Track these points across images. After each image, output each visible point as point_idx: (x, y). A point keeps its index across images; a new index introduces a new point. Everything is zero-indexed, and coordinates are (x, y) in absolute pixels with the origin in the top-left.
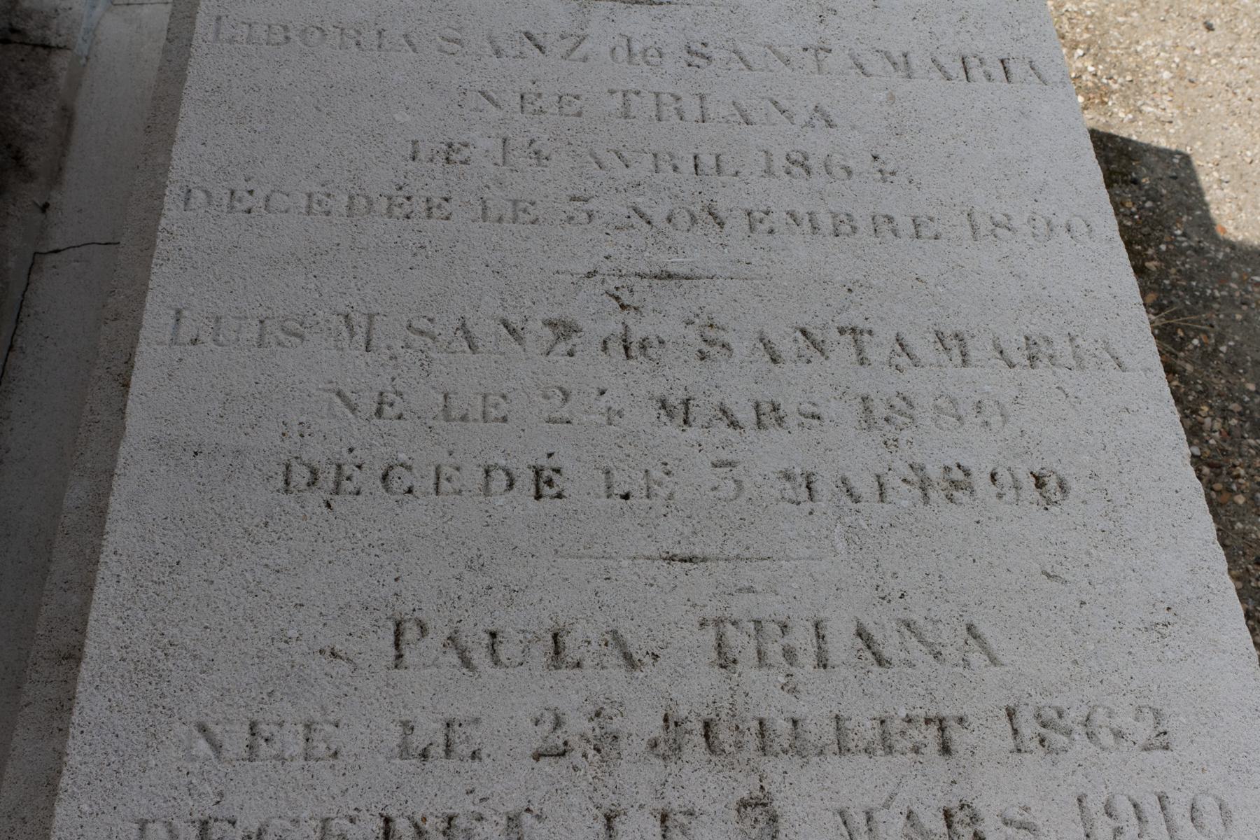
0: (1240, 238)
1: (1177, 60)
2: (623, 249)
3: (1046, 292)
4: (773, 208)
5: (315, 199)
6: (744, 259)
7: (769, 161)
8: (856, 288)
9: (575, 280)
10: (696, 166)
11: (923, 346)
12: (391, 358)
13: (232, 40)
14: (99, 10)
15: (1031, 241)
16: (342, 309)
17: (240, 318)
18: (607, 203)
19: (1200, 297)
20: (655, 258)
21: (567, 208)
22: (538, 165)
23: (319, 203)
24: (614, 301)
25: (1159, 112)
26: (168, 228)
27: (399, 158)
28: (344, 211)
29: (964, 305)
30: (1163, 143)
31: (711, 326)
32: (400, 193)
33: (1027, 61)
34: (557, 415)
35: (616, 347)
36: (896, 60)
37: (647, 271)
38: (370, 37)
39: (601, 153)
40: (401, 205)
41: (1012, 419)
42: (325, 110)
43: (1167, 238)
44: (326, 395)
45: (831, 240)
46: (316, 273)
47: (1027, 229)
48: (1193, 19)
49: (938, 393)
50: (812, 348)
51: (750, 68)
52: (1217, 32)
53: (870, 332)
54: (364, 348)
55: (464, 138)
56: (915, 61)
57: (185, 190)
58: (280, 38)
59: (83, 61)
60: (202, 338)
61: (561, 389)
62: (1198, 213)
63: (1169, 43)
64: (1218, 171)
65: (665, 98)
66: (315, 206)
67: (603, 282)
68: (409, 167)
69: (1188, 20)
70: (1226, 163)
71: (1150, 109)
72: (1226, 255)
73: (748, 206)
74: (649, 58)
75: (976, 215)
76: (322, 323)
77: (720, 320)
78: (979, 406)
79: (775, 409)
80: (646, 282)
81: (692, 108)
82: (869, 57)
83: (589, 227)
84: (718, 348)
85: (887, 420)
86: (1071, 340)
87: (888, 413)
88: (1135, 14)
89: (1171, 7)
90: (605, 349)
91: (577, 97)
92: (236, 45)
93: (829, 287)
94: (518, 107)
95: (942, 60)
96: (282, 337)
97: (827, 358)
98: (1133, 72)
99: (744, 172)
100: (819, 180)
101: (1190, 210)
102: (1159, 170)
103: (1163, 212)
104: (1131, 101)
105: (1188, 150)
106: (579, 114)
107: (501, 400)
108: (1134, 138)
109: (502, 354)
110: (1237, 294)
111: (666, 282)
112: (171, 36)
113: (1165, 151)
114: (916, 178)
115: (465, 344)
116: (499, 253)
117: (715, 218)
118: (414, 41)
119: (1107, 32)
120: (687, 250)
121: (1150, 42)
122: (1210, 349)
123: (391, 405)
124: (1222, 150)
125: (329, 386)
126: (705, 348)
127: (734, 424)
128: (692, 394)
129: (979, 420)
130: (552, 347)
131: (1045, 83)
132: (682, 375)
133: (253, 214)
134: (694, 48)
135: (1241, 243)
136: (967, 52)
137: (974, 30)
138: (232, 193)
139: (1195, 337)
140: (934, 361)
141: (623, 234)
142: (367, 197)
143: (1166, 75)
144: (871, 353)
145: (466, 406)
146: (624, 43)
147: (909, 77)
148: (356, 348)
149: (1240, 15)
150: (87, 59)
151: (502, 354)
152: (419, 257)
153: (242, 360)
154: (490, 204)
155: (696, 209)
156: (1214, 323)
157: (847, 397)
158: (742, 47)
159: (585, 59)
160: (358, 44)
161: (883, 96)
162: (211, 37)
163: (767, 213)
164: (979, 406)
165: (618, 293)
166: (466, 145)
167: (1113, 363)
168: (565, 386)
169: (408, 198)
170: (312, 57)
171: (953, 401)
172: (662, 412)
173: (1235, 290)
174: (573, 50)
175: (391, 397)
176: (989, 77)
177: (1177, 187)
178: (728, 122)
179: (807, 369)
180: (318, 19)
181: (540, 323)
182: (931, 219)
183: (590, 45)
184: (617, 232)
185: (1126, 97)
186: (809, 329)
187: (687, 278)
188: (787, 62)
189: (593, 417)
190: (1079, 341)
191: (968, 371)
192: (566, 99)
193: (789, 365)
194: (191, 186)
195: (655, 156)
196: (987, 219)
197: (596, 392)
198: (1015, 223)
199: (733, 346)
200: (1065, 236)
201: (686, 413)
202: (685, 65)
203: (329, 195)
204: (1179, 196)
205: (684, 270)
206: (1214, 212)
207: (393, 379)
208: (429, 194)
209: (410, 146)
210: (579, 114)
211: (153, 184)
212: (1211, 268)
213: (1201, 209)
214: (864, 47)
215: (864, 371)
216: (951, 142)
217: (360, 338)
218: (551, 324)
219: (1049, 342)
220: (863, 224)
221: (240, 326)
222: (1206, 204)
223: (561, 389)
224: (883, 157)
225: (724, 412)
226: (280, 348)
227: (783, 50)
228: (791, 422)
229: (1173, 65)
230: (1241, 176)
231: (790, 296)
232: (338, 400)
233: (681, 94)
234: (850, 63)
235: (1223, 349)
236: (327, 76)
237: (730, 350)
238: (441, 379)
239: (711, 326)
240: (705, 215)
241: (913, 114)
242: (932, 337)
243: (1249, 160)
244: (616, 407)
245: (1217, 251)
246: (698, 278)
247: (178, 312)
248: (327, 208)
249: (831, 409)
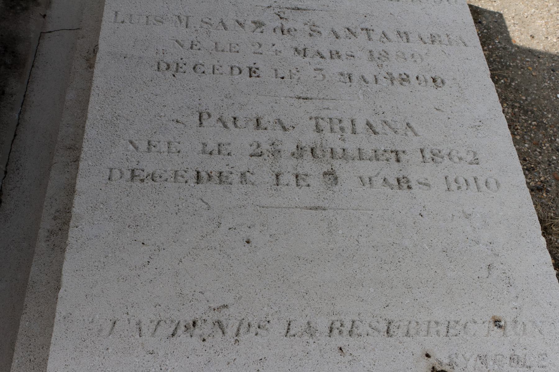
0: (521, 45)
8: (368, 16)
16: (177, 14)
30: (492, 9)
43: (492, 43)
53: (373, 30)
61: (258, 43)
70: (517, 17)
72: (515, 50)
78: (413, 55)
79: (337, 53)
80: (289, 10)
96: (155, 22)
108: (480, 7)
113: (492, 12)
126: (312, 32)
132: (303, 41)
135: (522, 46)
164: (413, 55)
168: (260, 42)
175: (196, 43)
177: (497, 25)
179: (349, 41)
193: (342, 40)
197: (271, 45)
199: (322, 32)
205: (304, 7)
206: (511, 35)
212: (509, 55)
215: (370, 42)
217: (184, 23)
218: (255, 23)
219: (439, 36)
228: (344, 57)
230: (523, 22)
235: (513, 84)
242: (396, 33)
245: (512, 49)
247: (116, 12)
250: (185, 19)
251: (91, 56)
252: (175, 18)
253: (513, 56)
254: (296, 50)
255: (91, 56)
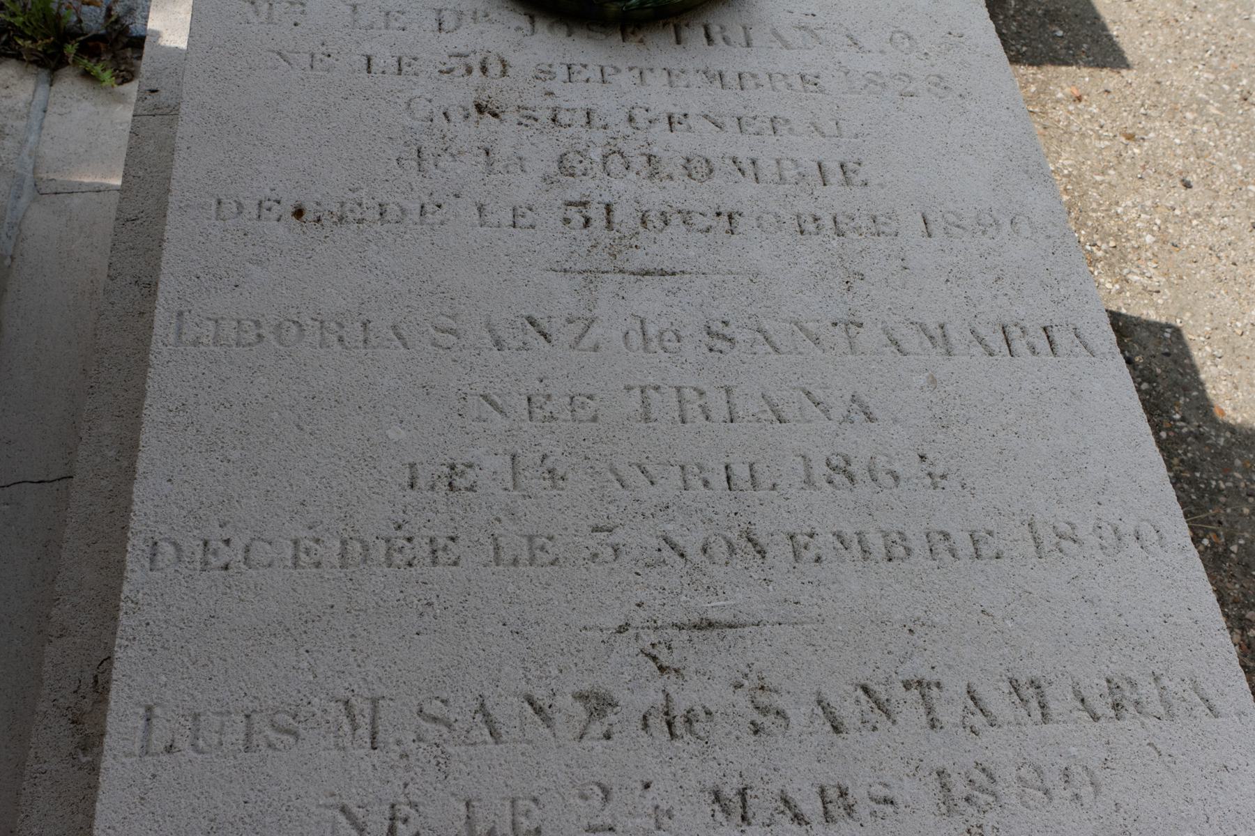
0: (1239, 420)
1: (1158, 222)
2: (655, 593)
3: (1122, 621)
4: (818, 530)
5: (302, 548)
6: (792, 598)
7: (808, 467)
8: (918, 629)
9: (605, 637)
10: (728, 478)
11: (998, 700)
12: (401, 756)
13: (197, 342)
14: (24, 200)
15: (1100, 556)
16: (342, 694)
17: (221, 714)
18: (634, 533)
19: (1205, 490)
20: (692, 603)
21: (590, 542)
22: (554, 487)
23: (307, 552)
24: (652, 663)
25: (1146, 281)
26: (132, 595)
27: (396, 488)
28: (336, 561)
29: (1037, 644)
30: (1153, 316)
31: (762, 688)
32: (399, 533)
33: (1071, 327)
34: (598, 822)
35: (658, 723)
36: (933, 334)
37: (685, 620)
38: (354, 331)
39: (623, 469)
40: (401, 550)
41: (1104, 789)
42: (307, 428)
43: (1166, 425)
44: (329, 813)
45: (884, 564)
46: (308, 646)
47: (1094, 540)
48: (1170, 175)
49: (1020, 760)
50: (876, 710)
51: (777, 350)
52: (1195, 189)
53: (938, 685)
54: (369, 745)
55: (468, 458)
56: (954, 336)
57: (150, 543)
58: (251, 337)
59: (8, 262)
60: (179, 744)
61: (599, 785)
62: (1195, 393)
63: (1149, 203)
64: (1210, 345)
65: (689, 394)
66: (303, 556)
67: (637, 637)
68: (408, 499)
69: (1164, 177)
70: (1218, 336)
71: (1136, 278)
72: (1227, 441)
73: (790, 529)
74: (667, 344)
75: (1038, 526)
76: (319, 713)
77: (772, 680)
78: (1066, 775)
79: (843, 794)
80: (684, 635)
81: (719, 410)
82: (904, 331)
83: (615, 565)
84: (772, 717)
85: (967, 800)
86: (1156, 679)
87: (968, 790)
88: (1112, 172)
89: (1147, 162)
90: (646, 726)
91: (590, 397)
92: (202, 348)
93: (888, 629)
94: (526, 413)
95: (982, 331)
96: (273, 735)
97: (894, 722)
98: (1116, 238)
99: (783, 484)
100: (864, 490)
101: (1186, 390)
102: (1151, 347)
103: (1159, 395)
104: (1117, 270)
105: (1178, 323)
106: (595, 419)
107: (533, 805)
108: (1124, 311)
109: (530, 742)
110: (1242, 485)
111: (708, 633)
112: (112, 272)
113: (1155, 324)
114: (968, 482)
115: (486, 732)
116: (516, 608)
117: (755, 545)
118: (404, 333)
119: (1085, 193)
120: (729, 592)
121: (1129, 203)
122: (1220, 549)
123: (405, 821)
124: (1212, 321)
125: (331, 801)
126: (759, 718)
127: (798, 818)
128: (748, 782)
129: (1068, 794)
130: (585, 728)
131: (1092, 354)
132: (736, 757)
133: (230, 571)
134: (714, 329)
135: (1241, 426)
136: (1007, 320)
137: (1011, 293)
138: (206, 544)
139: (1205, 536)
140: (1012, 719)
141: (654, 572)
142: (362, 542)
143: (1149, 239)
144: (942, 712)
145: (492, 817)
146: (638, 326)
147: (949, 353)
148: (360, 747)
149: (1216, 170)
150: (12, 258)
151: (530, 742)
152: (426, 618)
153: (227, 772)
154: (502, 541)
155: (733, 536)
156: (1223, 519)
157: (921, 773)
158: (766, 325)
159: (596, 348)
160: (341, 339)
161: (922, 379)
162: (172, 338)
163: (811, 536)
164: (1066, 775)
165: (654, 652)
166: (470, 466)
167: (1203, 707)
168: (604, 781)
169: (409, 540)
170: (289, 360)
171: (1038, 770)
172: (716, 807)
173: (1240, 480)
174: (581, 336)
175: (405, 810)
176: (1033, 351)
177: (1171, 365)
178: (758, 420)
179: (873, 738)
180: (294, 311)
181: (570, 698)
182: (990, 533)
183: (600, 331)
184: (647, 570)
185: (1111, 265)
186: (872, 686)
187: (731, 627)
188: (817, 341)
189: (638, 821)
190: (1165, 681)
191: (1049, 728)
192: (578, 400)
193: (853, 735)
194: (156, 538)
195: (683, 468)
196: (1050, 530)
197: (640, 786)
198: (1081, 533)
199: (789, 713)
200: (1135, 546)
201: (744, 807)
202: (706, 350)
203: (317, 541)
204: (1174, 375)
205: (725, 617)
206: (1211, 392)
207: (406, 785)
208: (432, 533)
209: (407, 471)
210: (595, 419)
211: (98, 460)
212: (1214, 456)
213: (1198, 390)
214: (896, 318)
215: (936, 736)
216: (1001, 434)
217: (364, 732)
218: (581, 697)
219: (1133, 684)
220: (918, 544)
221: (223, 725)
222: (1202, 384)
223: (599, 785)
224: (930, 456)
225: (786, 802)
226: (270, 752)
227: (811, 326)
228: (862, 811)
229: (1155, 228)
230: (1234, 349)
231: (847, 643)
232: (342, 818)
233: (705, 388)
234: (885, 338)
235: (1234, 548)
236: (308, 383)
237: (785, 718)
238: (462, 782)
239: (762, 688)
240: (743, 542)
241: (958, 401)
242: (1006, 687)
243: (1239, 332)
244: (664, 806)
245: (1218, 436)
246: (744, 626)
247: (149, 709)
248: (317, 558)
249: (905, 791)
250: (367, 708)
251: (87, 705)
252: (335, 709)
253: (1222, 458)
254: (717, 796)
255: (87, 705)
